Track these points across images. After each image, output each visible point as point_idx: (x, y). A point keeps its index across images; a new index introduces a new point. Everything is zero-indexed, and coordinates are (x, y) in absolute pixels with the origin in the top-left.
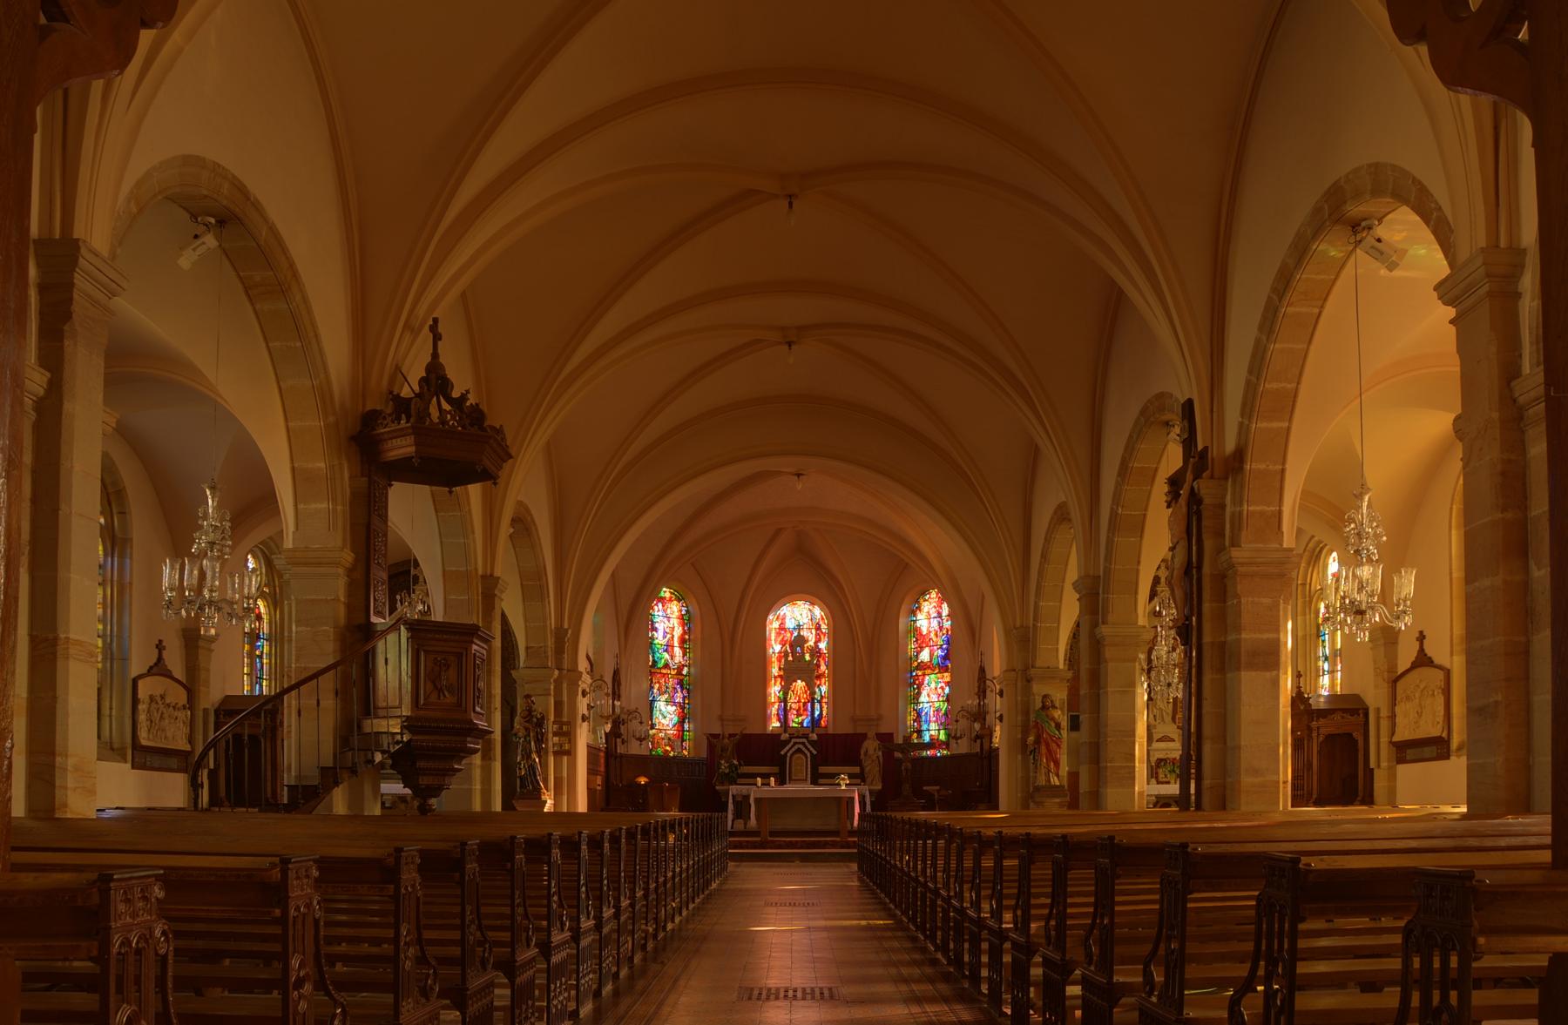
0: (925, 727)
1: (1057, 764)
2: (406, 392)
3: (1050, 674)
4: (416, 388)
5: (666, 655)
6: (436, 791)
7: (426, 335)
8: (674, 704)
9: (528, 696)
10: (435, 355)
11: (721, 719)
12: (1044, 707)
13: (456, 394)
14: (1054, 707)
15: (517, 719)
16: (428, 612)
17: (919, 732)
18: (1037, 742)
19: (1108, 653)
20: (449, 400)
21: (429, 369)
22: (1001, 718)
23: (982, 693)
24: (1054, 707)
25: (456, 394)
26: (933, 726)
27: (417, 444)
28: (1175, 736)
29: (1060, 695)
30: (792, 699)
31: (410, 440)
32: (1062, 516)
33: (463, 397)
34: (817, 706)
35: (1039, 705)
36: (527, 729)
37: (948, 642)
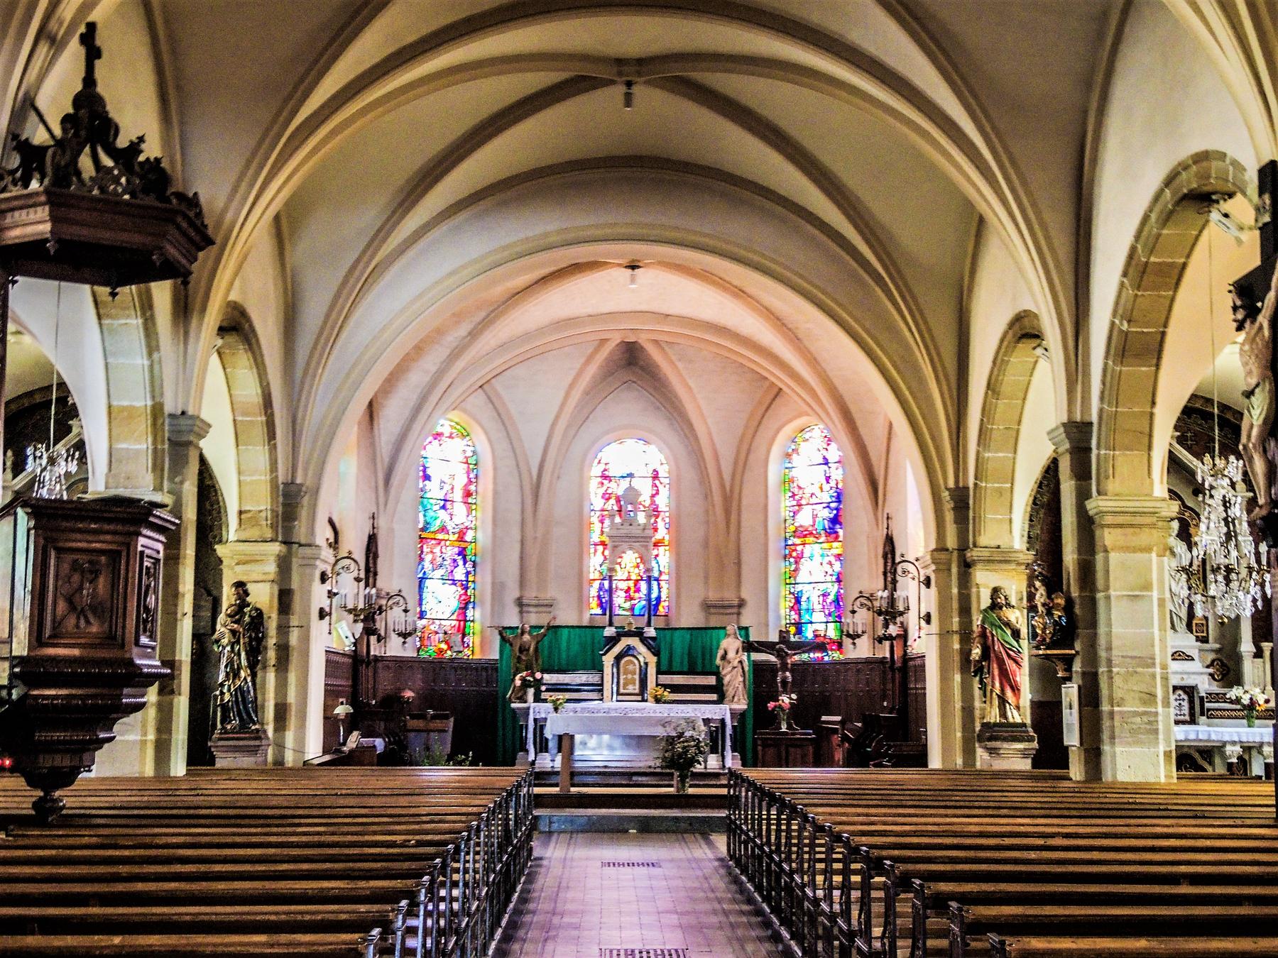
0: (806, 618)
1: (1016, 689)
2: (39, 137)
3: (1000, 558)
4: (58, 132)
5: (442, 513)
6: (67, 777)
7: (74, 51)
8: (454, 582)
9: (240, 585)
10: (89, 81)
11: (520, 603)
12: (995, 606)
13: (122, 142)
14: (1009, 605)
15: (222, 618)
16: (79, 481)
17: (799, 626)
18: (986, 654)
19: (1108, 537)
20: (112, 152)
21: (78, 101)
22: (928, 618)
23: (891, 581)
24: (1009, 605)
25: (122, 142)
26: (819, 617)
27: (54, 219)
28: (1194, 653)
29: (1014, 585)
30: (620, 574)
31: (43, 212)
32: (1024, 331)
33: (135, 148)
34: (655, 584)
35: (986, 602)
36: (233, 632)
37: (839, 498)
